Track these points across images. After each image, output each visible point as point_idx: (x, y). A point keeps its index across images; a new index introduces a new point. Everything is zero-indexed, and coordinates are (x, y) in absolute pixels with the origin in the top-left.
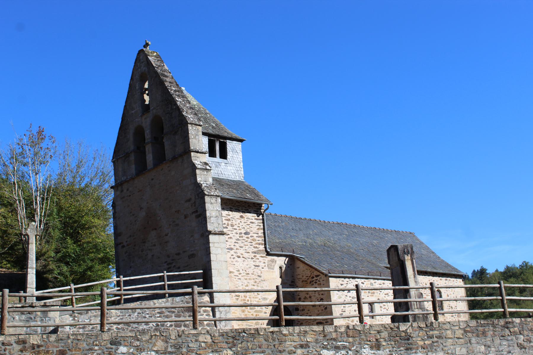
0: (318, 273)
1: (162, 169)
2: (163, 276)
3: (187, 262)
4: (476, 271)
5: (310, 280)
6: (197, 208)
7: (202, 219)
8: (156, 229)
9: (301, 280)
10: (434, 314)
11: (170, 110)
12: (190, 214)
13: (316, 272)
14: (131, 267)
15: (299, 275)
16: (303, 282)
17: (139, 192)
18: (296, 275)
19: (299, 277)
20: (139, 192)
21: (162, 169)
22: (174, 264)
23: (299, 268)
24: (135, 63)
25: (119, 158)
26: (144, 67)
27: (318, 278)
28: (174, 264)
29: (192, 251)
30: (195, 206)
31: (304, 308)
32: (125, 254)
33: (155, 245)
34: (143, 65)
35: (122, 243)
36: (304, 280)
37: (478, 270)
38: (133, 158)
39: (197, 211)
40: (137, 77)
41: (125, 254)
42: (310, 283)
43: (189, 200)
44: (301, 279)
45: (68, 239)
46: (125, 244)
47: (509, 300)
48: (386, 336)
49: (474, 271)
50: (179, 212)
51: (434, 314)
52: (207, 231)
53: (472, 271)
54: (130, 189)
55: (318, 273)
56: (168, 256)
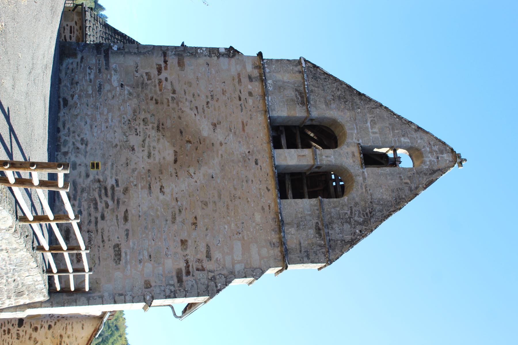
1: (269, 190)
3: (109, 240)
4: (106, 20)
6: (193, 276)
8: (175, 161)
9: (63, 333)
14: (122, 85)
15: (72, 328)
16: (61, 336)
17: (243, 123)
18: (72, 323)
19: (69, 327)
20: (243, 123)
21: (269, 190)
22: (110, 203)
23: (83, 328)
25: (303, 78)
26: (430, 161)
28: (110, 203)
29: (126, 254)
30: (198, 270)
31: (21, 339)
32: (147, 74)
33: (149, 156)
34: (433, 159)
35: (166, 68)
36: (63, 340)
37: (107, 21)
38: (297, 115)
39: (188, 273)
40: (419, 141)
41: (147, 74)
43: (209, 256)
44: (66, 333)
46: (163, 76)
47: (40, 303)
49: (107, 18)
50: (194, 227)
53: (107, 15)
54: (250, 101)
56: (126, 190)
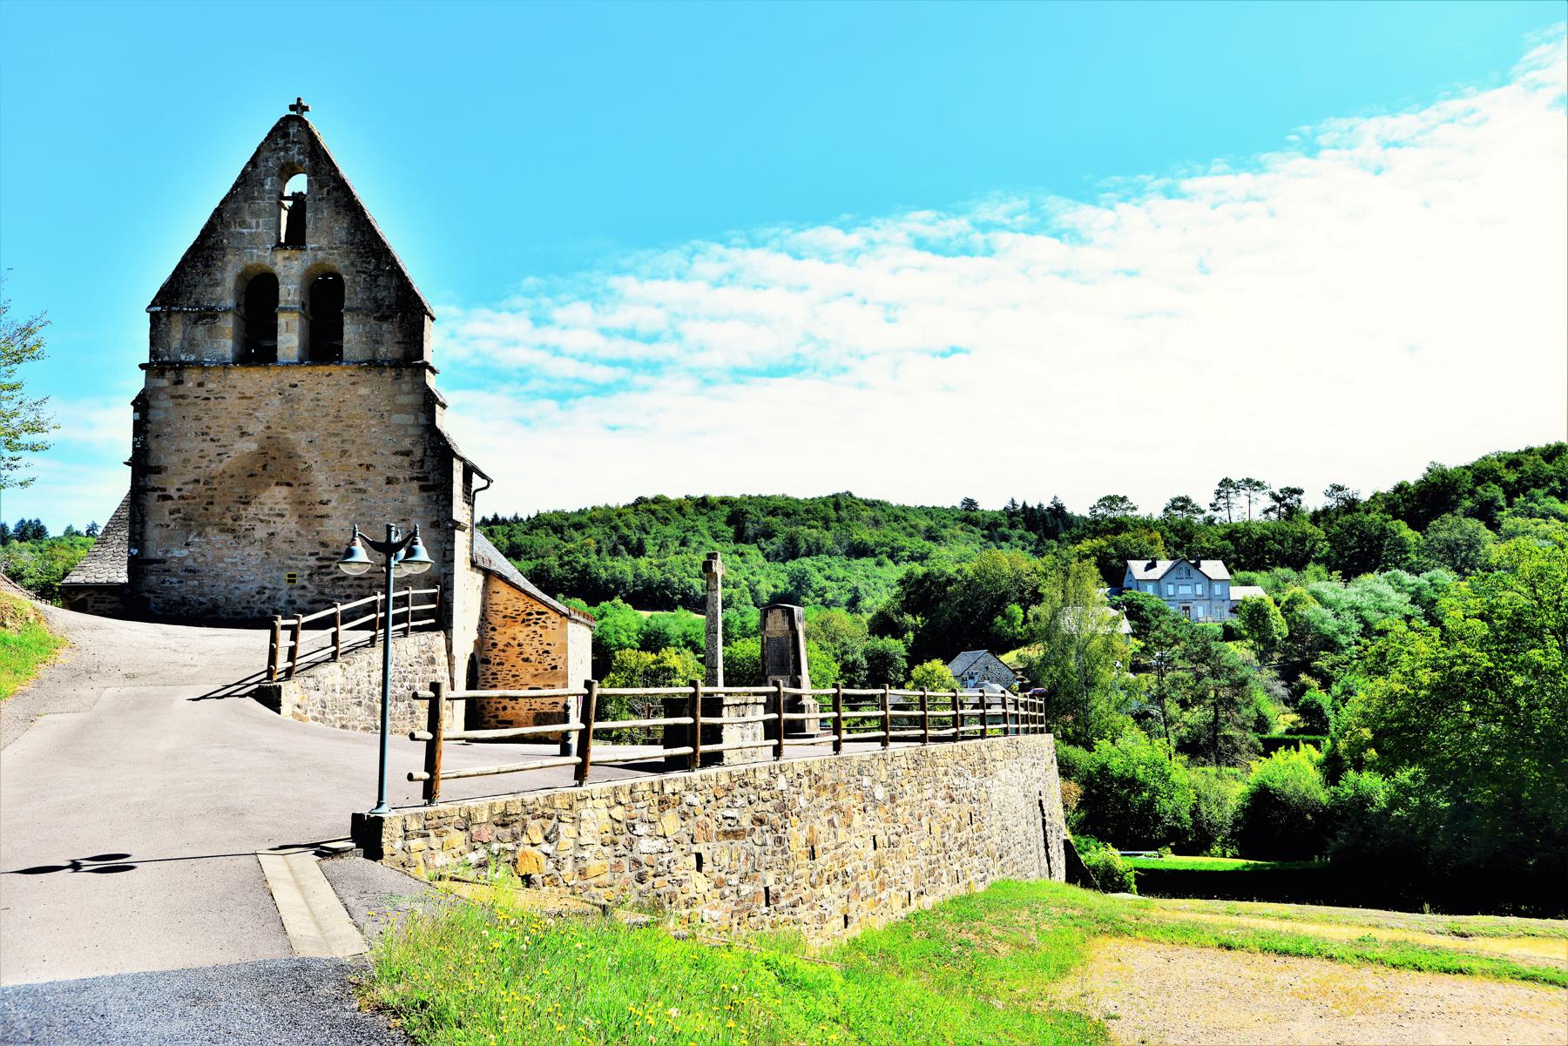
0: (544, 609)
2: (408, 595)
5: (524, 616)
7: (438, 496)
8: (289, 485)
9: (502, 614)
10: (428, 742)
11: (371, 268)
12: (404, 478)
13: (540, 606)
16: (505, 617)
17: (240, 398)
19: (495, 608)
20: (240, 398)
21: (330, 374)
24: (270, 135)
27: (543, 617)
41: (171, 514)
42: (523, 621)
45: (1536, 769)
46: (172, 492)
48: (1238, 672)
49: (23, 521)
50: (371, 468)
51: (428, 742)
52: (451, 519)
55: (544, 609)
